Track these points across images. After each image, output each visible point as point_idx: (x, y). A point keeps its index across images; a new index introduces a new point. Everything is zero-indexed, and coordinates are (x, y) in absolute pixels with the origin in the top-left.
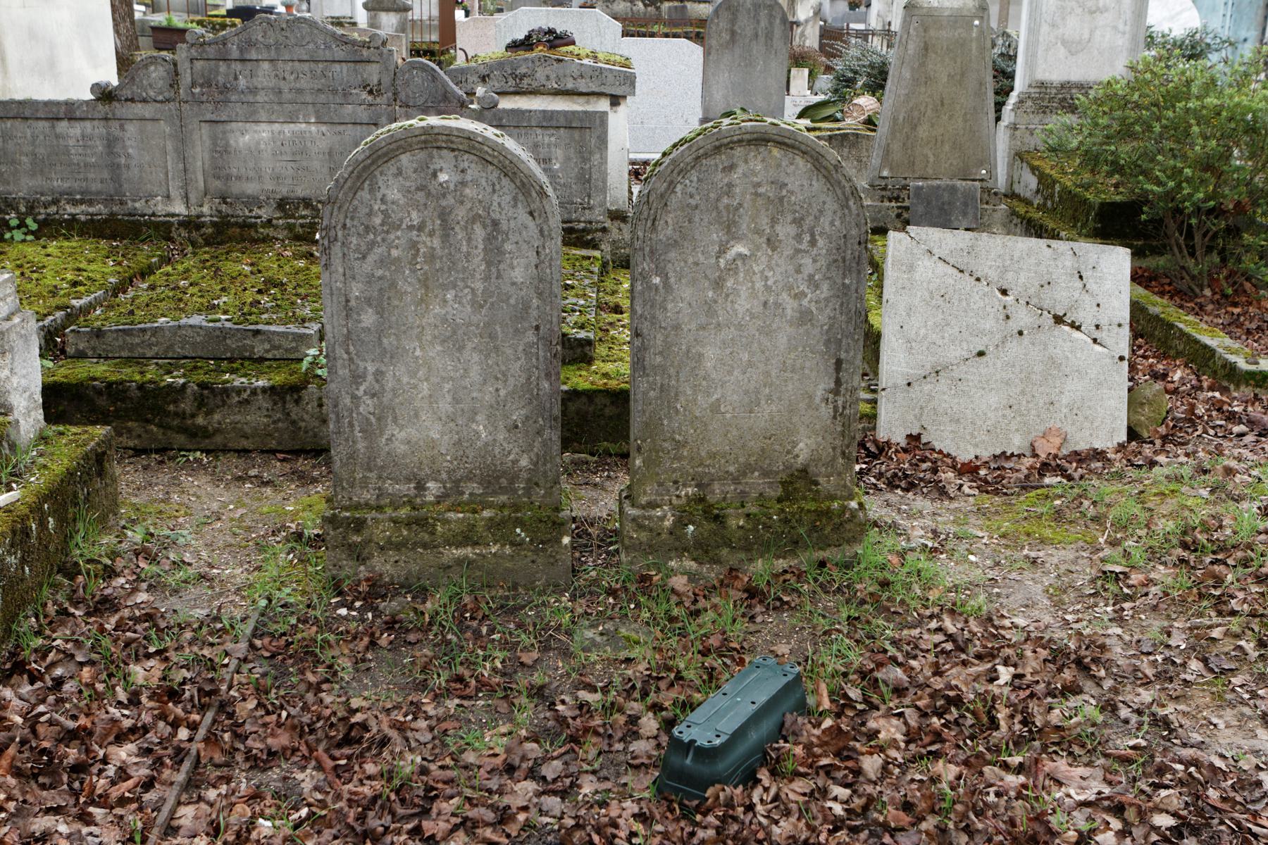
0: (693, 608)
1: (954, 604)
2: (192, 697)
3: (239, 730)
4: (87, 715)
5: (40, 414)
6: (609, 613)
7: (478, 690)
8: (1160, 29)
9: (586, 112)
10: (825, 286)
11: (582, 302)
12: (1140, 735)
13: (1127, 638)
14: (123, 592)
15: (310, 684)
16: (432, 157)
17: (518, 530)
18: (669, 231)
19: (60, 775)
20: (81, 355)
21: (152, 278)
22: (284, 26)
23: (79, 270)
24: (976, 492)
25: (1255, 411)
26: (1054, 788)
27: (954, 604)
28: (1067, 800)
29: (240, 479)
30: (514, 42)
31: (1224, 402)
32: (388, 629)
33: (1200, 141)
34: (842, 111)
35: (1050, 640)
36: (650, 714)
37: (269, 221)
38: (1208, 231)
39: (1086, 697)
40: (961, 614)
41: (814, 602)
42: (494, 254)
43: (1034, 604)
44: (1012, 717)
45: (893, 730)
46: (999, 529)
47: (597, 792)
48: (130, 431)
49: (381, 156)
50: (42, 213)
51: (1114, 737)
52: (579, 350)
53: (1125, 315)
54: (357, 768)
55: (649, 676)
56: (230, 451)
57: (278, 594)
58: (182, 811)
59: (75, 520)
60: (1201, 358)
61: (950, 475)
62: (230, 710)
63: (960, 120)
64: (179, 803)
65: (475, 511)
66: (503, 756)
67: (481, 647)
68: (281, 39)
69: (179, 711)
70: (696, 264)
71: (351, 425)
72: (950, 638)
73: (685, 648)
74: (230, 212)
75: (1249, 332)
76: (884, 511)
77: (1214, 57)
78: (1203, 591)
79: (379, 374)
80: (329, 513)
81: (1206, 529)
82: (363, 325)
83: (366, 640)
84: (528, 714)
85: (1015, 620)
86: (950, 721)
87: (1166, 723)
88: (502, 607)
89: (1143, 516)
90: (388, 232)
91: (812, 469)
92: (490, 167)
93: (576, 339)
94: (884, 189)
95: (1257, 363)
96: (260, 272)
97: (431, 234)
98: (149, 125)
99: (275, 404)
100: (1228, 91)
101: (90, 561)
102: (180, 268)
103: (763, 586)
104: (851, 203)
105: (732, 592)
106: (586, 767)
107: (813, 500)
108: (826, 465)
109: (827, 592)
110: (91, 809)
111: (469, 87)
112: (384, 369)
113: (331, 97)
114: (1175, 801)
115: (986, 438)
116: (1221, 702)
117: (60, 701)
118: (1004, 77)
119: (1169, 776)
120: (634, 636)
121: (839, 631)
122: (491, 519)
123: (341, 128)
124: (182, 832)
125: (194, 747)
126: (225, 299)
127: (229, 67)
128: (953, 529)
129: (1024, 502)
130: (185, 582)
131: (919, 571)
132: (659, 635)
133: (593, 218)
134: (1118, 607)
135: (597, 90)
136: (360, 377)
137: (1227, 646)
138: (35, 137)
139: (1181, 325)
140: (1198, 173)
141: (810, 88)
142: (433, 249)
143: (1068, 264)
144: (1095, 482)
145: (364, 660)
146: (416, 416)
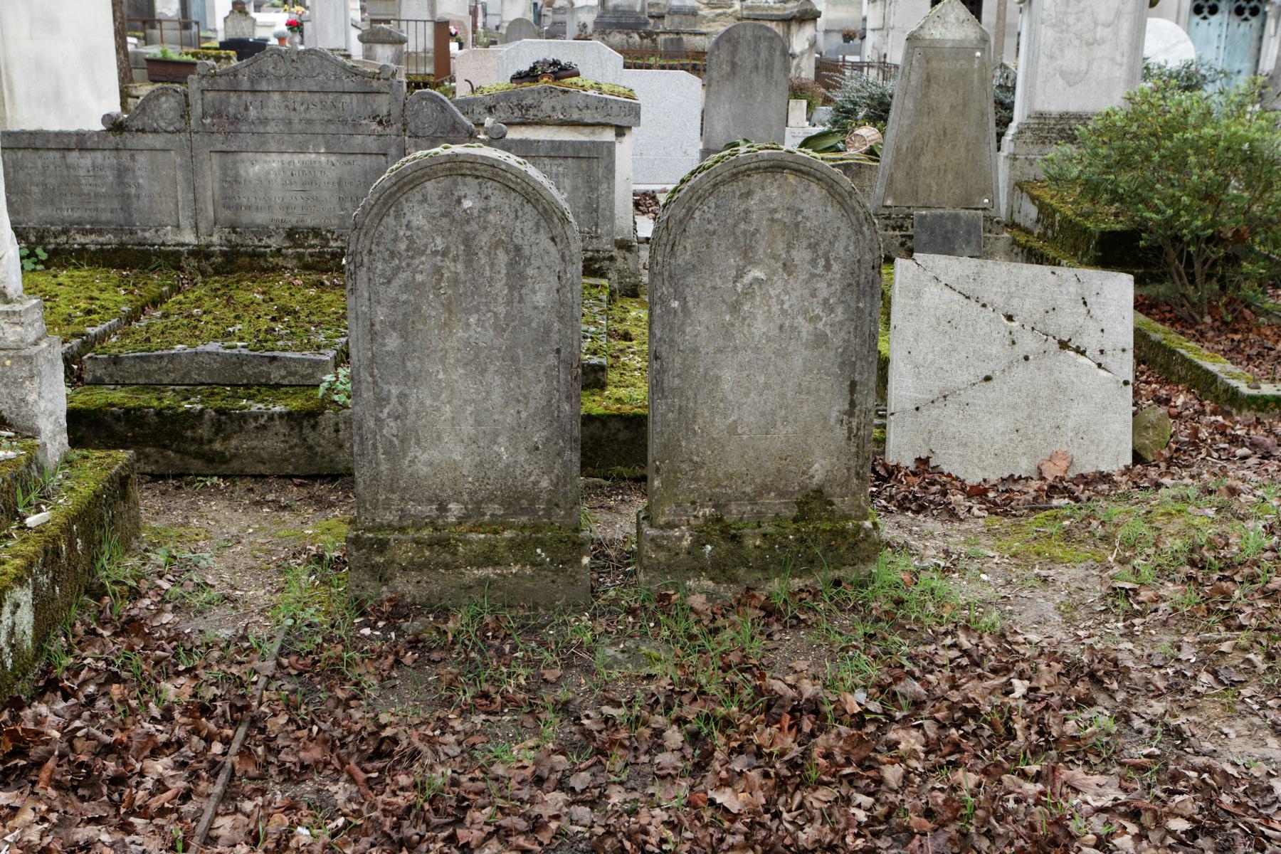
0: (711, 626)
1: (968, 621)
2: (224, 712)
3: (272, 745)
4: (122, 730)
5: (64, 438)
6: (629, 631)
7: (503, 706)
8: (1156, 61)
9: (593, 143)
10: (840, 310)
11: (593, 329)
12: (1154, 744)
13: (1138, 652)
14: (148, 614)
15: (339, 700)
16: (456, 184)
17: (539, 551)
18: (688, 256)
19: (100, 787)
20: (98, 382)
21: (164, 306)
22: (295, 57)
23: (92, 298)
24: (986, 514)
25: (1258, 434)
26: (1072, 796)
27: (968, 621)
28: (1084, 806)
29: (258, 504)
30: (519, 73)
31: (1227, 427)
32: (411, 648)
33: (1196, 170)
34: (844, 142)
35: (1063, 655)
36: (675, 727)
37: (279, 250)
38: (1207, 259)
39: (1100, 709)
40: (975, 630)
41: (830, 619)
42: (517, 279)
43: (1047, 621)
44: (1028, 727)
45: (913, 741)
46: (1009, 548)
47: (625, 802)
48: (147, 456)
49: (408, 183)
50: (52, 243)
51: (1128, 746)
52: (592, 376)
53: (1129, 341)
54: (388, 780)
55: (672, 690)
56: (246, 476)
57: (302, 615)
58: (220, 821)
59: (100, 542)
60: (1203, 383)
61: (960, 497)
62: (261, 725)
63: (962, 150)
64: (217, 814)
65: (496, 532)
66: (532, 769)
67: (504, 665)
68: (292, 71)
69: (212, 725)
70: (714, 288)
71: (375, 447)
72: (965, 653)
73: (705, 664)
74: (239, 241)
75: (1249, 358)
76: (895, 533)
77: (1209, 89)
78: (1212, 606)
79: (403, 397)
80: (352, 534)
81: (1213, 547)
82: (388, 348)
83: (391, 658)
84: (554, 729)
85: (1029, 636)
86: (967, 731)
87: (1178, 732)
88: (523, 626)
89: (1151, 535)
90: (412, 257)
91: (827, 490)
92: (514, 194)
93: (589, 365)
94: (888, 218)
95: (1258, 388)
96: (272, 300)
97: (455, 259)
98: (160, 155)
99: (292, 429)
100: (1224, 122)
101: (116, 583)
102: (192, 296)
103: (780, 604)
104: (865, 228)
105: (749, 611)
106: (613, 778)
107: (829, 519)
108: (841, 485)
109: (842, 611)
110: (132, 819)
111: (475, 118)
112: (407, 392)
113: (341, 127)
114: (1190, 806)
115: (994, 462)
116: (1231, 713)
117: (94, 717)
118: (1004, 108)
119: (1183, 783)
120: (654, 653)
121: (855, 647)
122: (512, 539)
123: (351, 158)
124: (220, 841)
125: (229, 761)
126: (239, 326)
127: (239, 98)
128: (965, 549)
129: (1033, 523)
130: (209, 603)
131: (932, 590)
132: (680, 653)
133: (600, 247)
134: (1128, 623)
135: (602, 121)
136: (384, 400)
137: (1236, 658)
138: (45, 168)
139: (1183, 352)
140: (1196, 202)
141: (809, 119)
142: (457, 274)
143: (1072, 290)
144: (1103, 503)
145: (389, 678)
146: (439, 438)
